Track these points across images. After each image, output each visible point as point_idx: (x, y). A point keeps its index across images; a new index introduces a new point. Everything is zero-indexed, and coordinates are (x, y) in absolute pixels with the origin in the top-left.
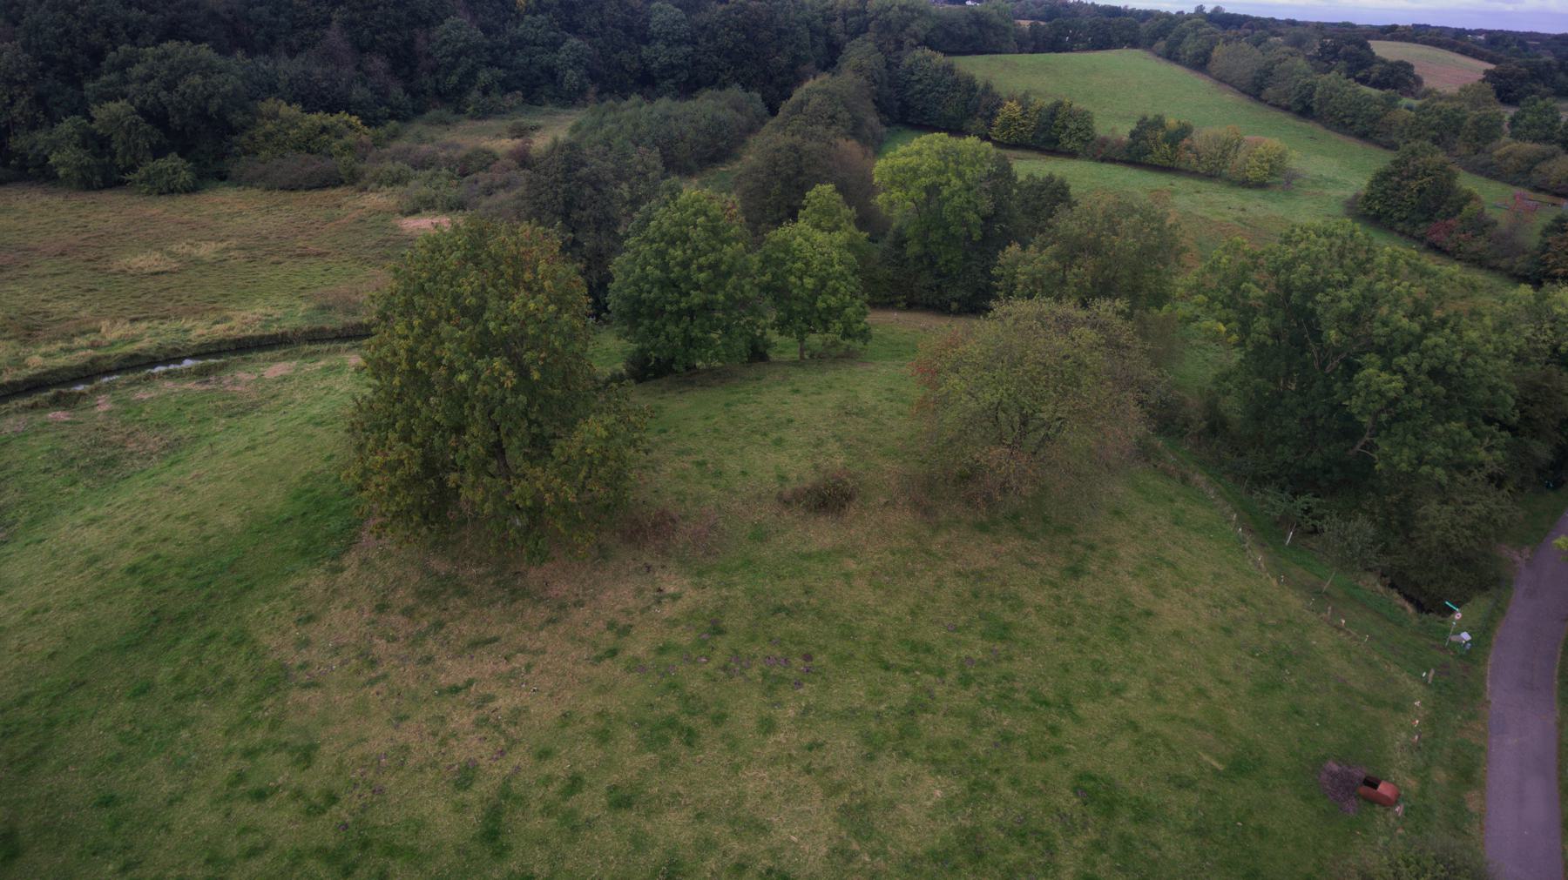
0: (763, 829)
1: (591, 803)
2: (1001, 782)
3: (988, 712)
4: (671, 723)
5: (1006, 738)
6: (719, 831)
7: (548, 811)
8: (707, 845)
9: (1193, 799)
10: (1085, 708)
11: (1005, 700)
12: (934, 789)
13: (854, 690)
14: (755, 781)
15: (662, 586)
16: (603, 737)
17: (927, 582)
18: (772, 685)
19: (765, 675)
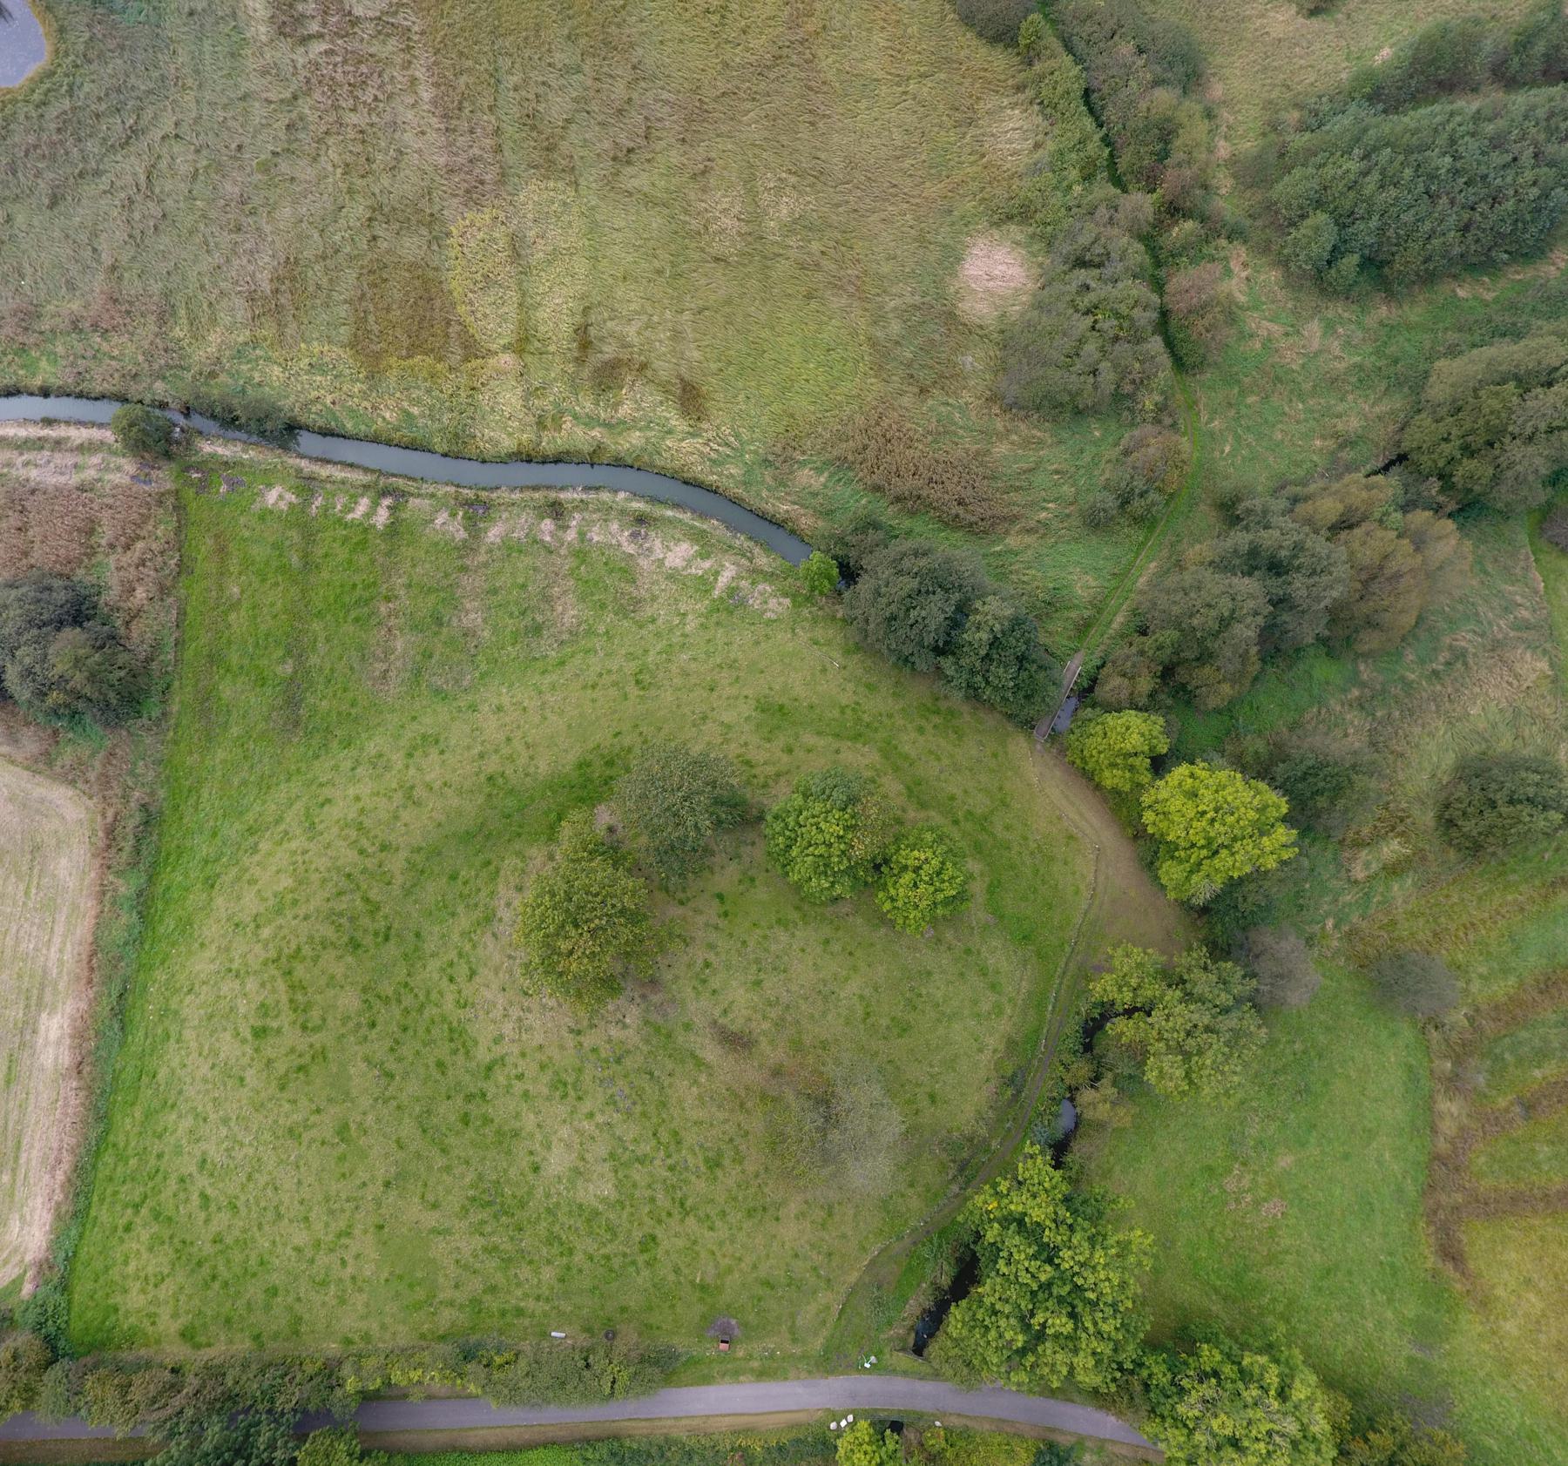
0: (549, 1148)
1: (518, 1087)
2: (628, 1209)
3: (658, 1186)
4: (565, 1084)
5: (653, 1200)
6: (539, 1137)
7: (508, 1076)
8: (532, 1135)
9: (672, 1277)
10: (691, 1220)
11: (670, 1189)
12: (607, 1189)
13: (630, 1131)
14: (565, 1132)
15: (535, 1044)
16: (543, 1067)
17: (721, 1116)
18: (611, 1101)
19: (612, 1096)
